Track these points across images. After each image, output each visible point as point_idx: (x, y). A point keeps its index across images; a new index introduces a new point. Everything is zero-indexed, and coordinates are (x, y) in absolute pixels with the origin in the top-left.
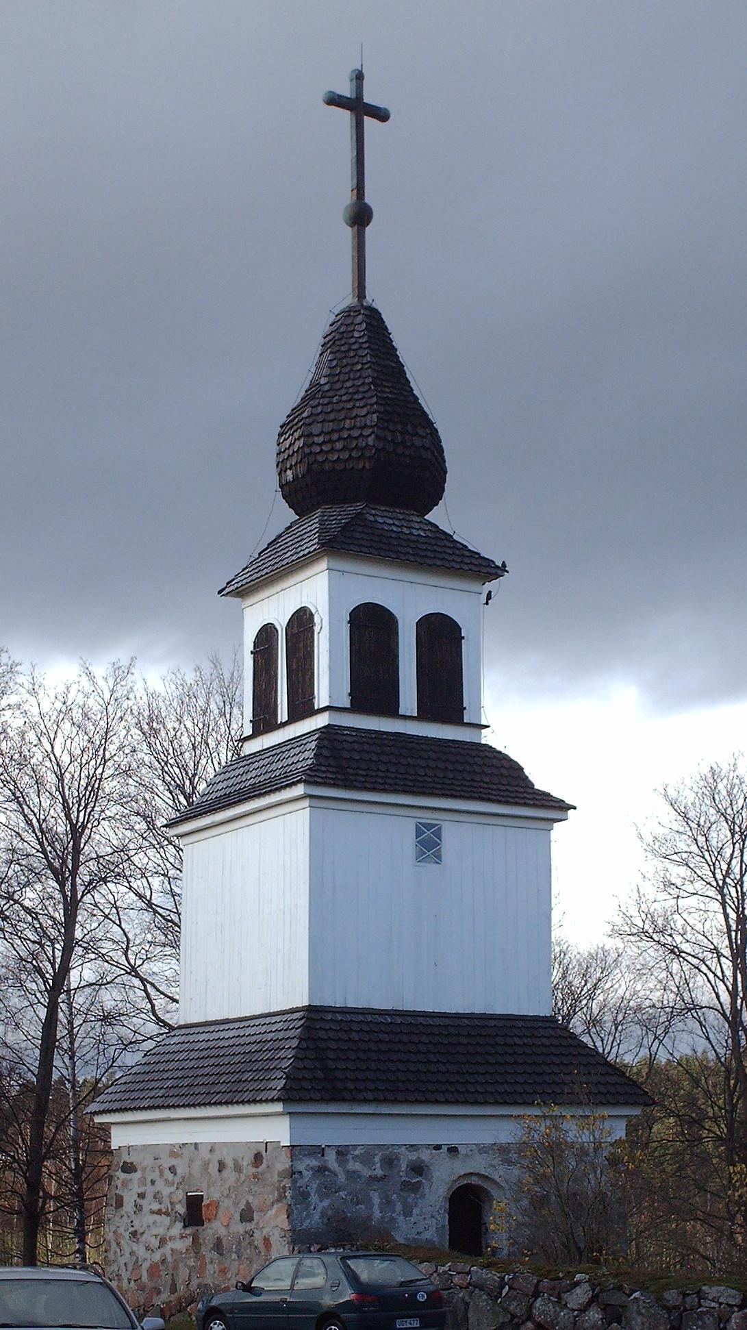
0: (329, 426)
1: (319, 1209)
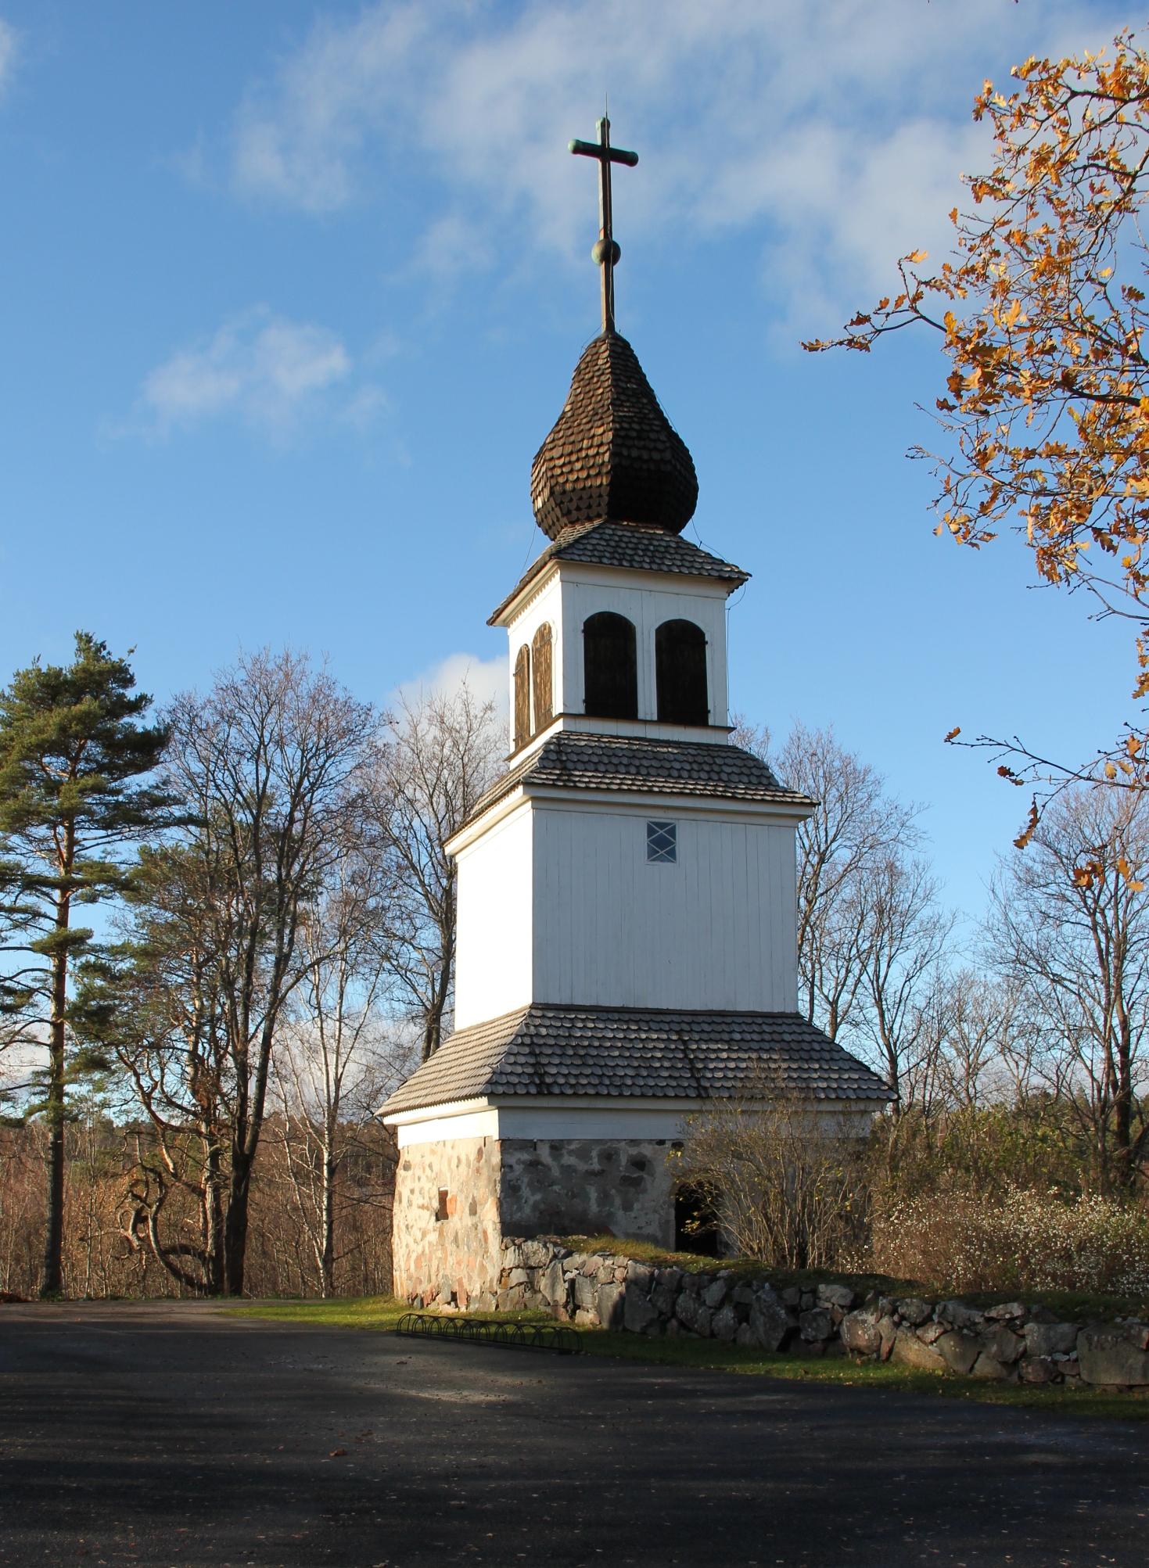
0: (568, 449)
1: (531, 1202)
